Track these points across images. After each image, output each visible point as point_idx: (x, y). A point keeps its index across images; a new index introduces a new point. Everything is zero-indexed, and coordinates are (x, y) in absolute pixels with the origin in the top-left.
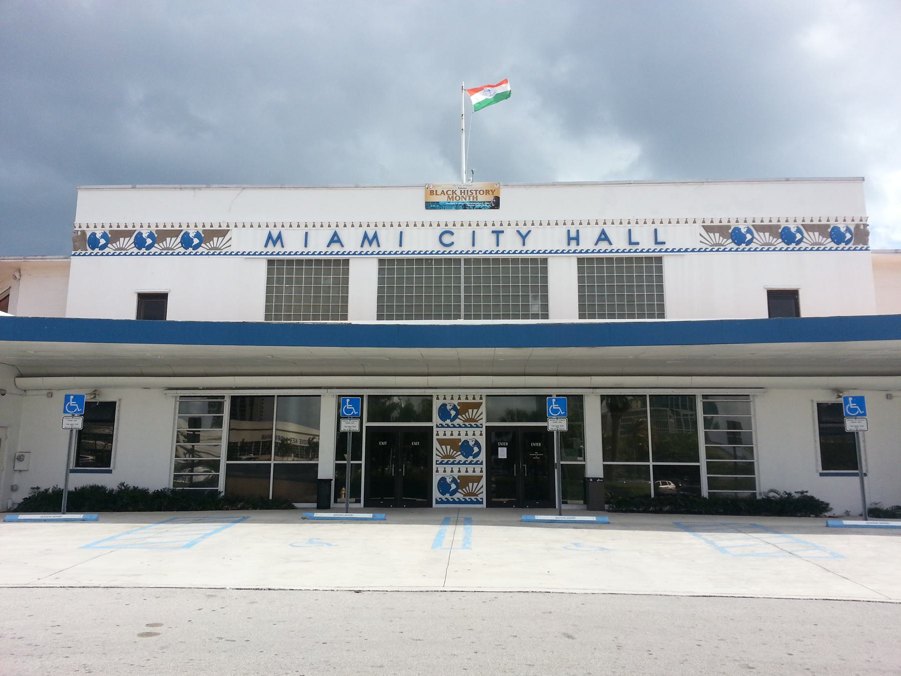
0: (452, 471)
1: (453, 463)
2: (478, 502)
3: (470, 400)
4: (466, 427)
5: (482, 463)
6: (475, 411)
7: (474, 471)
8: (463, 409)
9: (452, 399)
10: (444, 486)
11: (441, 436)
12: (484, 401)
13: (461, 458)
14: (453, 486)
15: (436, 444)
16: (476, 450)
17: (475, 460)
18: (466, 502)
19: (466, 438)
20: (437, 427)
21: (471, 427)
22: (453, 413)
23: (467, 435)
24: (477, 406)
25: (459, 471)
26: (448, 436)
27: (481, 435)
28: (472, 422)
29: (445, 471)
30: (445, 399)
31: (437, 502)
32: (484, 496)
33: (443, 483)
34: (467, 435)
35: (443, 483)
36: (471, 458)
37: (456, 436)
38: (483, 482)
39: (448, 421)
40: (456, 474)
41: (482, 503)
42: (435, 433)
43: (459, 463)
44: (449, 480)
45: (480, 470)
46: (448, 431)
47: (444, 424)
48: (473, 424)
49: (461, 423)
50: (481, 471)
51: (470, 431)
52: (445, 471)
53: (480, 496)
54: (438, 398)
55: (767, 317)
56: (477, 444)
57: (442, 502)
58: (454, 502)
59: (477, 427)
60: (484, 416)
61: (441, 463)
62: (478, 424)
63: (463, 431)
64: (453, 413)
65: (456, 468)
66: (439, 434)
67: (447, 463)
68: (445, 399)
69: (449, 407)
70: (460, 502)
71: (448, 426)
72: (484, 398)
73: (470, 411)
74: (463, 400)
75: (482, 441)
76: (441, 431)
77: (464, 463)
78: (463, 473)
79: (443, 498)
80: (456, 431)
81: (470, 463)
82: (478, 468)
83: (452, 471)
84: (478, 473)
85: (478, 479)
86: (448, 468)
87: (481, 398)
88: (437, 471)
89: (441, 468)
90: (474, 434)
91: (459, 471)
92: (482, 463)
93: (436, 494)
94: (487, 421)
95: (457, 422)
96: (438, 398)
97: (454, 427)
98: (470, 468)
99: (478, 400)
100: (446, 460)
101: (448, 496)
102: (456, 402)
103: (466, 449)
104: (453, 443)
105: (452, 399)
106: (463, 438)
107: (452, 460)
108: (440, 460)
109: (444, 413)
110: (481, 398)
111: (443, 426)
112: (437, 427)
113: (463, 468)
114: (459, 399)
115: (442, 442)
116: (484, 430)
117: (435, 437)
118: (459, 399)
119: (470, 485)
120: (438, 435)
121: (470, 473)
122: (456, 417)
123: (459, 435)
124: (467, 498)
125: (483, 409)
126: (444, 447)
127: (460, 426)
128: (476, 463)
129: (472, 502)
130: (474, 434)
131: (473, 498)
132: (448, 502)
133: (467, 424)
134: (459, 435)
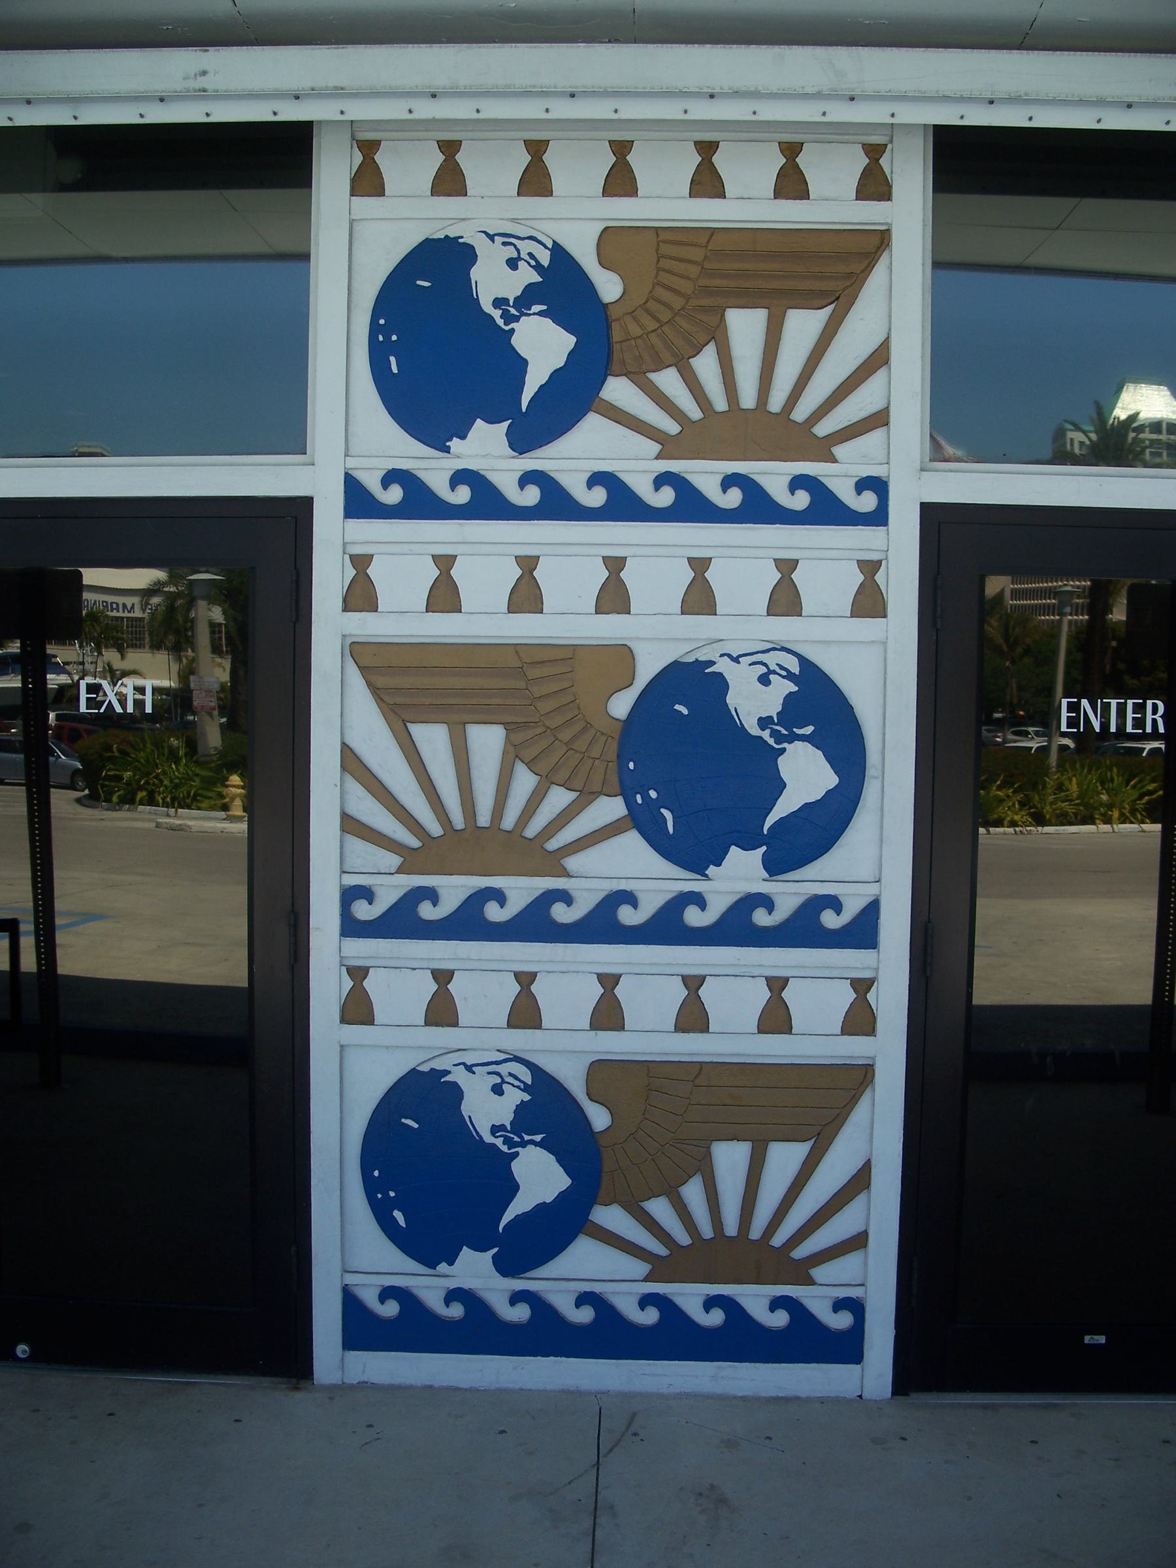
0: (525, 1013)
1: (535, 924)
2: (806, 1340)
3: (749, 201)
4: (691, 506)
5: (863, 931)
6: (802, 326)
7: (776, 1018)
8: (645, 308)
9: (536, 181)
10: (430, 1165)
11: (402, 617)
12: (909, 210)
13: (635, 868)
14: (539, 1177)
15: (340, 712)
16: (805, 775)
17: (789, 893)
18: (674, 1337)
19: (426, 1048)
20: (359, 502)
21: (758, 508)
22: (543, 345)
23: (699, 599)
24: (832, 270)
25: (608, 1015)
26: (483, 619)
27: (869, 602)
28: (765, 479)
29: (442, 1012)
30: (449, 181)
31: (362, 1331)
32: (876, 1277)
33: (418, 1111)
34: (699, 599)
35: (418, 1111)
36: (740, 871)
37: (569, 616)
38: (877, 1131)
39: (485, 447)
40: (567, 1048)
41: (847, 1347)
42: (328, 578)
43: (602, 925)
44: (487, 1110)
45: (846, 1012)
46: (486, 556)
47: (435, 471)
48: (774, 477)
49: (638, 466)
50: (860, 1020)
51: (744, 559)
52: (442, 1012)
53: (836, 1276)
54: (368, 181)
55: (570, 341)
56: (819, 708)
57: (413, 1328)
58: (545, 1333)
59: (826, 509)
60: (907, 387)
61: (402, 922)
62: (840, 477)
63: (657, 556)
64: (543, 345)
65: (568, 977)
66: (376, 589)
67: (468, 923)
68: (449, 181)
69: (493, 281)
70: (607, 1335)
71: (487, 502)
72: (912, 176)
73: (745, 326)
74: (663, 197)
75: (882, 673)
76: (402, 556)
77: (667, 927)
78: (650, 1034)
79: (431, 1288)
80: (570, 558)
81: (738, 927)
82: (819, 986)
83: (525, 1013)
84: (817, 1037)
85: (815, 1101)
86: (485, 975)
87: (874, 185)
88: (358, 1009)
89: (401, 976)
90: (785, 600)
91: (608, 1015)
92: (863, 931)
93: (349, 1246)
94: (956, 428)
95: (584, 451)
96: (368, 181)
97: (556, 504)
98: (735, 983)
99: (833, 202)
100: (454, 890)
101: (474, 1269)
102: (576, 218)
103: (690, 761)
104: (524, 691)
105: (536, 181)
106: (657, 637)
107: (520, 890)
108: (390, 889)
109: (435, 340)
110: (874, 185)
111: (419, 502)
112: (359, 502)
113: (652, 978)
114: (620, 181)
115: (410, 684)
116: (900, 548)
117: (330, 626)
118: (620, 181)
119: (730, 1158)
120: (360, 595)
121: (734, 1034)
122: (571, 397)
123: (614, 597)
124: (690, 1297)
125: (898, 302)
126: (432, 739)
127: (623, 504)
128: (803, 929)
129: (739, 1339)
130: (785, 600)
131: (755, 1299)
132: (476, 1330)
133: (706, 475)
134: (614, 597)
